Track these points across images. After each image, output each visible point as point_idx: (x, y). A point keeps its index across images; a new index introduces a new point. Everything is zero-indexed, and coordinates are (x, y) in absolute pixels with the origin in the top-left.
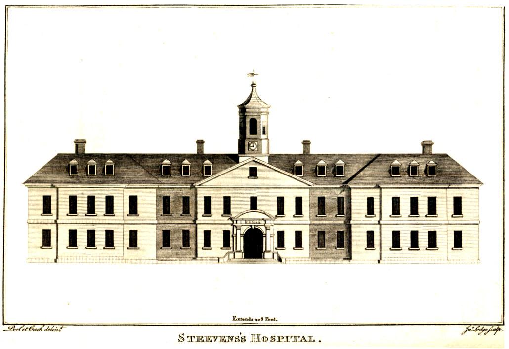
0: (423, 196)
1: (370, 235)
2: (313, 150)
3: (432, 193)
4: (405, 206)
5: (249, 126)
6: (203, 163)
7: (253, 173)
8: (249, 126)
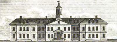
0: (91, 27)
1: (84, 35)
2: (72, 17)
3: (97, 26)
4: (91, 29)
5: (58, 11)
6: (48, 21)
7: (59, 22)
8: (58, 11)
